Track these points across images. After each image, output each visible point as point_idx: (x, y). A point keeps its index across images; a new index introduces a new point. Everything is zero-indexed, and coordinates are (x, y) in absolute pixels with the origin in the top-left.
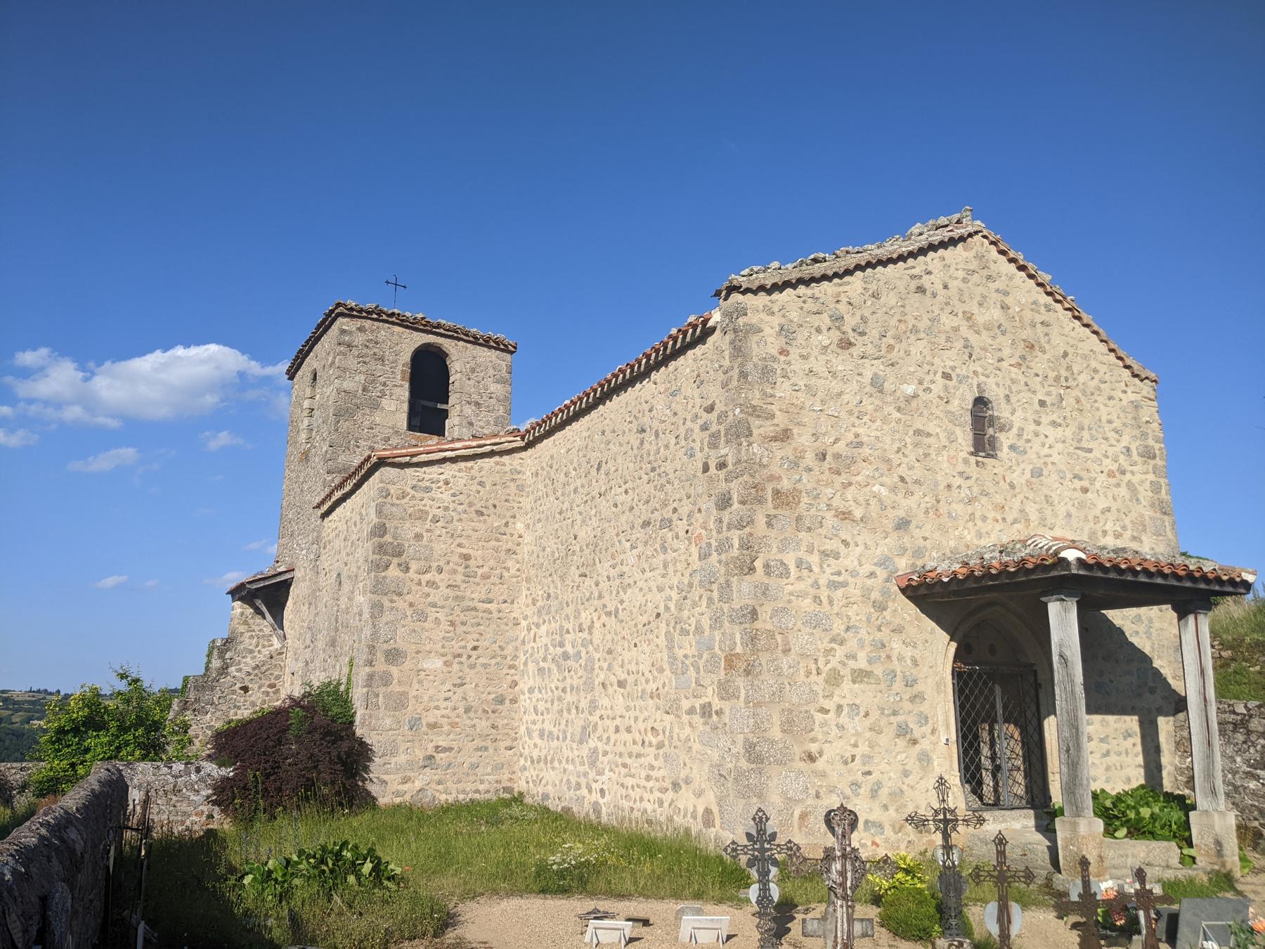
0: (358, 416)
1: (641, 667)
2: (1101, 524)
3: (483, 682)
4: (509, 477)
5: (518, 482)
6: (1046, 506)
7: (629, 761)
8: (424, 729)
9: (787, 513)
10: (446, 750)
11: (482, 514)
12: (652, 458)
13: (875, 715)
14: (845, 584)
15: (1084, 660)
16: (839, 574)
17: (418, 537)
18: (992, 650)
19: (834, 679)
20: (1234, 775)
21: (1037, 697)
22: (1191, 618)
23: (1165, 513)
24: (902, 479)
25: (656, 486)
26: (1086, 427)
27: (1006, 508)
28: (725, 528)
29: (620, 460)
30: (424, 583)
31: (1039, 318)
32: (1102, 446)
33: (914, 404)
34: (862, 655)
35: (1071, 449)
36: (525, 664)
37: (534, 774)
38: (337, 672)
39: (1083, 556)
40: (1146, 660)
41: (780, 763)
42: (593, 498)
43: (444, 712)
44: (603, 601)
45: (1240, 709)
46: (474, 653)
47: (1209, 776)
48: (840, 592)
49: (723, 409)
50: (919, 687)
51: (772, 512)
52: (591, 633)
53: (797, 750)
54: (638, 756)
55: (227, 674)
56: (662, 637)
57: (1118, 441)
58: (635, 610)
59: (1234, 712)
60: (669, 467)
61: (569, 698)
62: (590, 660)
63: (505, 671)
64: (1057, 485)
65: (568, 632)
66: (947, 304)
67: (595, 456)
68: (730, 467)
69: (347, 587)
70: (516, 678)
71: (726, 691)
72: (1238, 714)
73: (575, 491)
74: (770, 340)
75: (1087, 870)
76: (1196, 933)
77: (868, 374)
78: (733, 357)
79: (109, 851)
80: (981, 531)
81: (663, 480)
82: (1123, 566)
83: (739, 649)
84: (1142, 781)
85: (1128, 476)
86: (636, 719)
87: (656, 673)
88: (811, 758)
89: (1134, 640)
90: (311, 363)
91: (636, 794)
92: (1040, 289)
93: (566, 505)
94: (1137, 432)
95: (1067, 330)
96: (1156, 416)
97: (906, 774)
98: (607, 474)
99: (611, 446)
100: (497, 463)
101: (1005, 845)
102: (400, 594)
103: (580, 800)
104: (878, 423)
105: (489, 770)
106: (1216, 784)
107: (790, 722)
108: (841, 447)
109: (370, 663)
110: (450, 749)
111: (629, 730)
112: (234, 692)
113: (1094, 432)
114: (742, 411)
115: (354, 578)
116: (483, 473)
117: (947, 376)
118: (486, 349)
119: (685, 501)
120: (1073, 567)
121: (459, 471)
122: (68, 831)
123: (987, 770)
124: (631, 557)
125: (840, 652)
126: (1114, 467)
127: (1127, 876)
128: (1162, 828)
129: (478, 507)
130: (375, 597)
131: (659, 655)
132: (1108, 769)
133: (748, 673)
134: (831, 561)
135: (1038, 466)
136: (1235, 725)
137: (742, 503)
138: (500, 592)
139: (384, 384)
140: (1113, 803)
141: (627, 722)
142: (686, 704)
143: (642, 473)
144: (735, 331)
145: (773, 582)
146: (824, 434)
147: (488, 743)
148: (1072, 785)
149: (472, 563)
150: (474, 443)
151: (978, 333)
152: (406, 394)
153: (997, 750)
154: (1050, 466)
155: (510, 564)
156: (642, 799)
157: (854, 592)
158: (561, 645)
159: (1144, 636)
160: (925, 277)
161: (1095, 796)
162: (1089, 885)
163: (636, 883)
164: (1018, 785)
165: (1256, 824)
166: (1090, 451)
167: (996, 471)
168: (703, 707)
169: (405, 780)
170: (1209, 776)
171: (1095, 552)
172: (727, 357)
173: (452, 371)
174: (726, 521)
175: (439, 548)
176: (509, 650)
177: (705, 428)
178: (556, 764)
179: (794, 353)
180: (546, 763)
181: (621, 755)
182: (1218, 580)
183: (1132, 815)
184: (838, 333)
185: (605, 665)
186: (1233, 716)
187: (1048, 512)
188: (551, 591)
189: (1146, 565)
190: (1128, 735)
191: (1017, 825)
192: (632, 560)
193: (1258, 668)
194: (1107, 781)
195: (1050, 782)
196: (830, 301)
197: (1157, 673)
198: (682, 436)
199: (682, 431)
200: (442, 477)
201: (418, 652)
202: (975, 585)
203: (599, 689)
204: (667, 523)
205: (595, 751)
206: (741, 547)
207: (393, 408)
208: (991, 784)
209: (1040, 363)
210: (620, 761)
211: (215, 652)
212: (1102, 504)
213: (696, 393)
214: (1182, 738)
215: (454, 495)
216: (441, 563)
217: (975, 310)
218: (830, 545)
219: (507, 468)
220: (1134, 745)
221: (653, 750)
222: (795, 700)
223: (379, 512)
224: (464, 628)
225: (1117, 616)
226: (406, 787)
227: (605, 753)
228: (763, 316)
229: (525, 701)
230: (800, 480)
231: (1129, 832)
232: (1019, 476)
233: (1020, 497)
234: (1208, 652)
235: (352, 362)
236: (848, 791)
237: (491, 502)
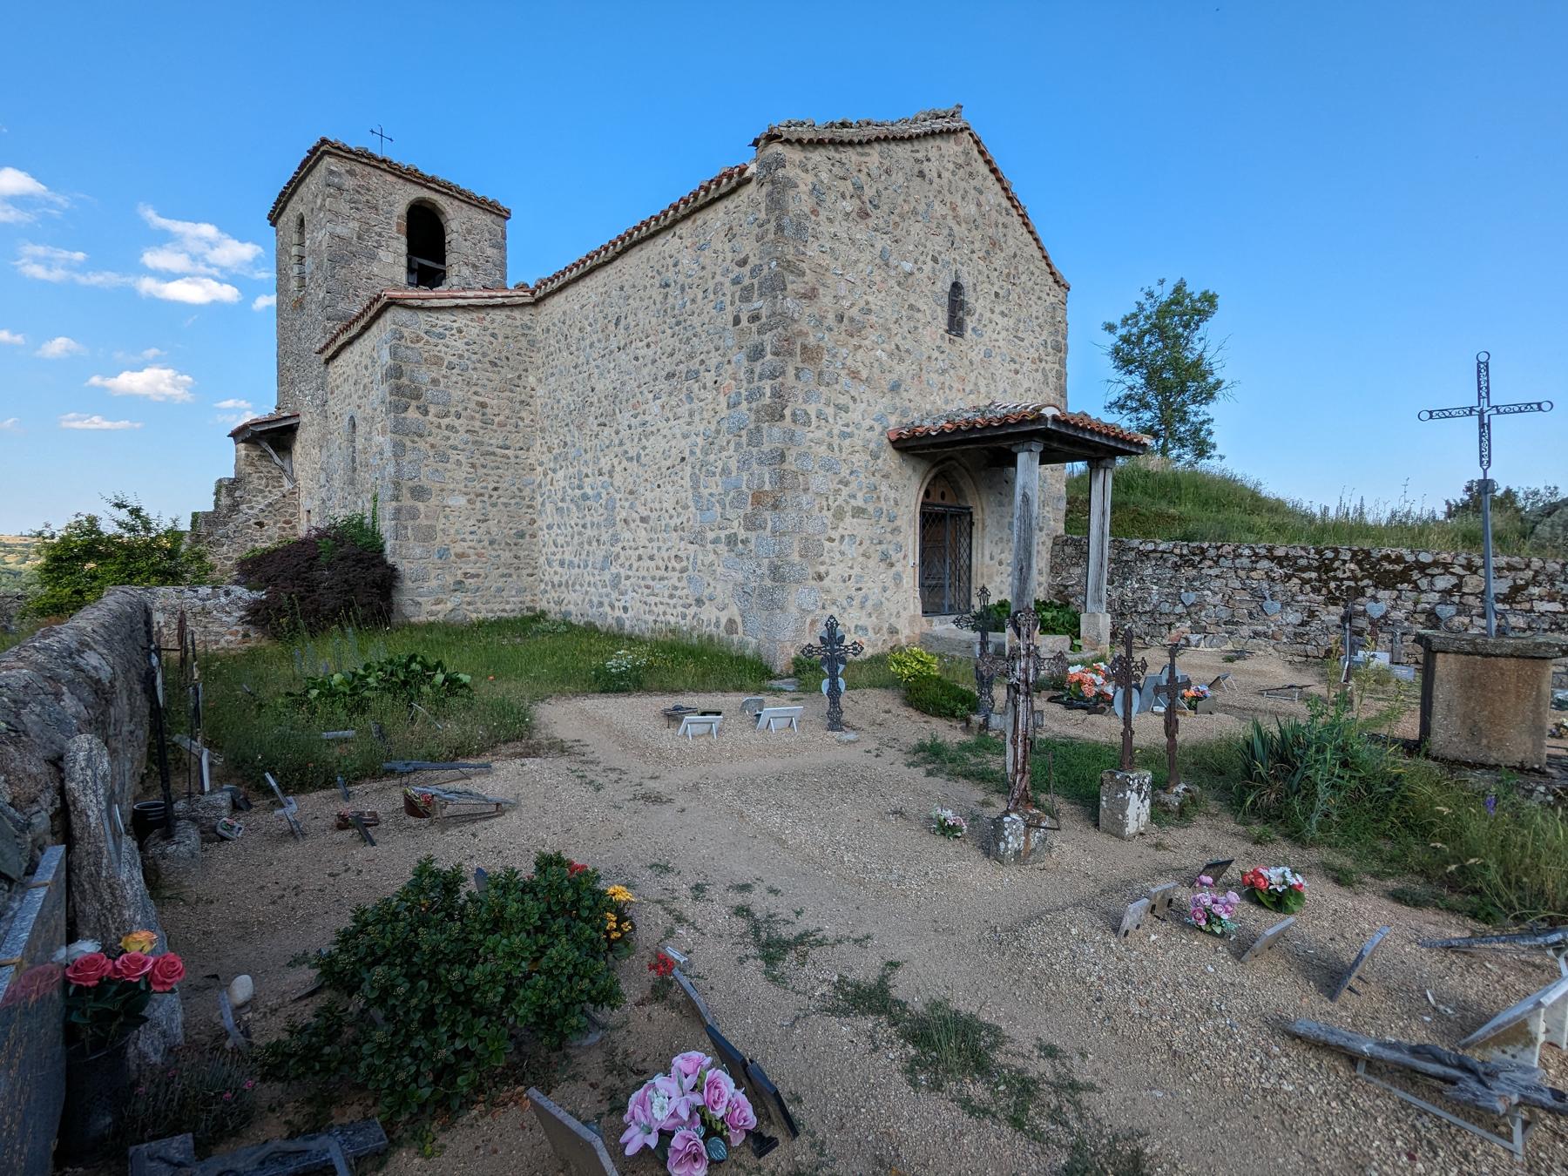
0: (355, 264)
1: (665, 505)
3: (505, 519)
4: (519, 331)
5: (529, 338)
7: (651, 583)
8: (453, 558)
9: (812, 368)
10: (473, 576)
11: (496, 365)
12: (676, 312)
13: (867, 543)
14: (850, 435)
16: (847, 425)
17: (435, 382)
19: (839, 514)
24: (897, 347)
25: (681, 340)
28: (756, 378)
29: (641, 315)
30: (443, 427)
31: (1001, 220)
33: (910, 281)
34: (860, 495)
36: (543, 504)
37: (556, 596)
38: (363, 506)
39: (1058, 413)
41: (798, 582)
42: (612, 352)
43: (471, 544)
44: (624, 447)
46: (495, 494)
48: (848, 441)
49: (758, 262)
50: (897, 523)
51: (800, 365)
52: (611, 477)
53: (810, 571)
54: (661, 579)
55: (239, 511)
56: (688, 478)
58: (658, 456)
60: (695, 320)
61: (589, 532)
62: (611, 499)
63: (524, 510)
65: (587, 476)
66: (940, 192)
67: (612, 312)
68: (764, 320)
69: (362, 428)
70: (534, 516)
71: (752, 523)
73: (592, 345)
74: (804, 197)
77: (879, 246)
78: (769, 210)
79: (154, 679)
81: (689, 333)
83: (767, 487)
86: (659, 548)
87: (680, 510)
88: (820, 578)
90: (295, 207)
91: (661, 609)
92: (1002, 192)
93: (582, 359)
94: (1052, 329)
95: (1019, 233)
97: (885, 589)
98: (626, 329)
99: (631, 301)
100: (508, 317)
102: (421, 436)
103: (604, 616)
104: (883, 294)
105: (514, 593)
107: (806, 548)
108: (854, 312)
109: (396, 498)
110: (478, 576)
111: (651, 558)
112: (249, 527)
114: (778, 265)
115: (370, 420)
116: (495, 325)
117: (935, 260)
118: (481, 211)
119: (713, 353)
121: (472, 320)
122: (85, 656)
124: (655, 407)
125: (845, 491)
129: (491, 357)
130: (398, 437)
131: (684, 494)
133: (775, 507)
134: (843, 414)
137: (776, 354)
138: (516, 440)
139: (380, 235)
141: (649, 552)
142: (710, 535)
143: (666, 326)
144: (773, 182)
145: (798, 429)
146: (843, 298)
147: (512, 571)
149: (488, 410)
150: (486, 294)
151: (959, 223)
152: (404, 249)
155: (524, 414)
156: (665, 613)
157: (859, 443)
158: (580, 487)
160: (925, 163)
163: (685, 681)
166: (1022, 340)
168: (728, 537)
169: (438, 602)
172: (763, 210)
173: (448, 231)
174: (758, 370)
175: (456, 394)
176: (527, 492)
177: (736, 281)
178: (578, 587)
179: (823, 214)
180: (567, 587)
181: (644, 578)
184: (858, 202)
185: (627, 504)
188: (568, 439)
192: (656, 410)
196: (853, 168)
198: (711, 290)
199: (711, 285)
200: (455, 325)
201: (442, 490)
203: (620, 525)
204: (694, 375)
205: (618, 576)
206: (773, 395)
207: (390, 260)
209: (999, 261)
210: (643, 583)
211: (224, 491)
213: (727, 246)
215: (467, 344)
216: (459, 409)
217: (959, 202)
218: (844, 400)
219: (518, 323)
221: (677, 574)
222: (811, 531)
223: (394, 354)
224: (485, 471)
226: (439, 607)
227: (628, 577)
228: (799, 171)
229: (544, 536)
232: (976, 356)
235: (344, 208)
236: (845, 603)
237: (504, 354)
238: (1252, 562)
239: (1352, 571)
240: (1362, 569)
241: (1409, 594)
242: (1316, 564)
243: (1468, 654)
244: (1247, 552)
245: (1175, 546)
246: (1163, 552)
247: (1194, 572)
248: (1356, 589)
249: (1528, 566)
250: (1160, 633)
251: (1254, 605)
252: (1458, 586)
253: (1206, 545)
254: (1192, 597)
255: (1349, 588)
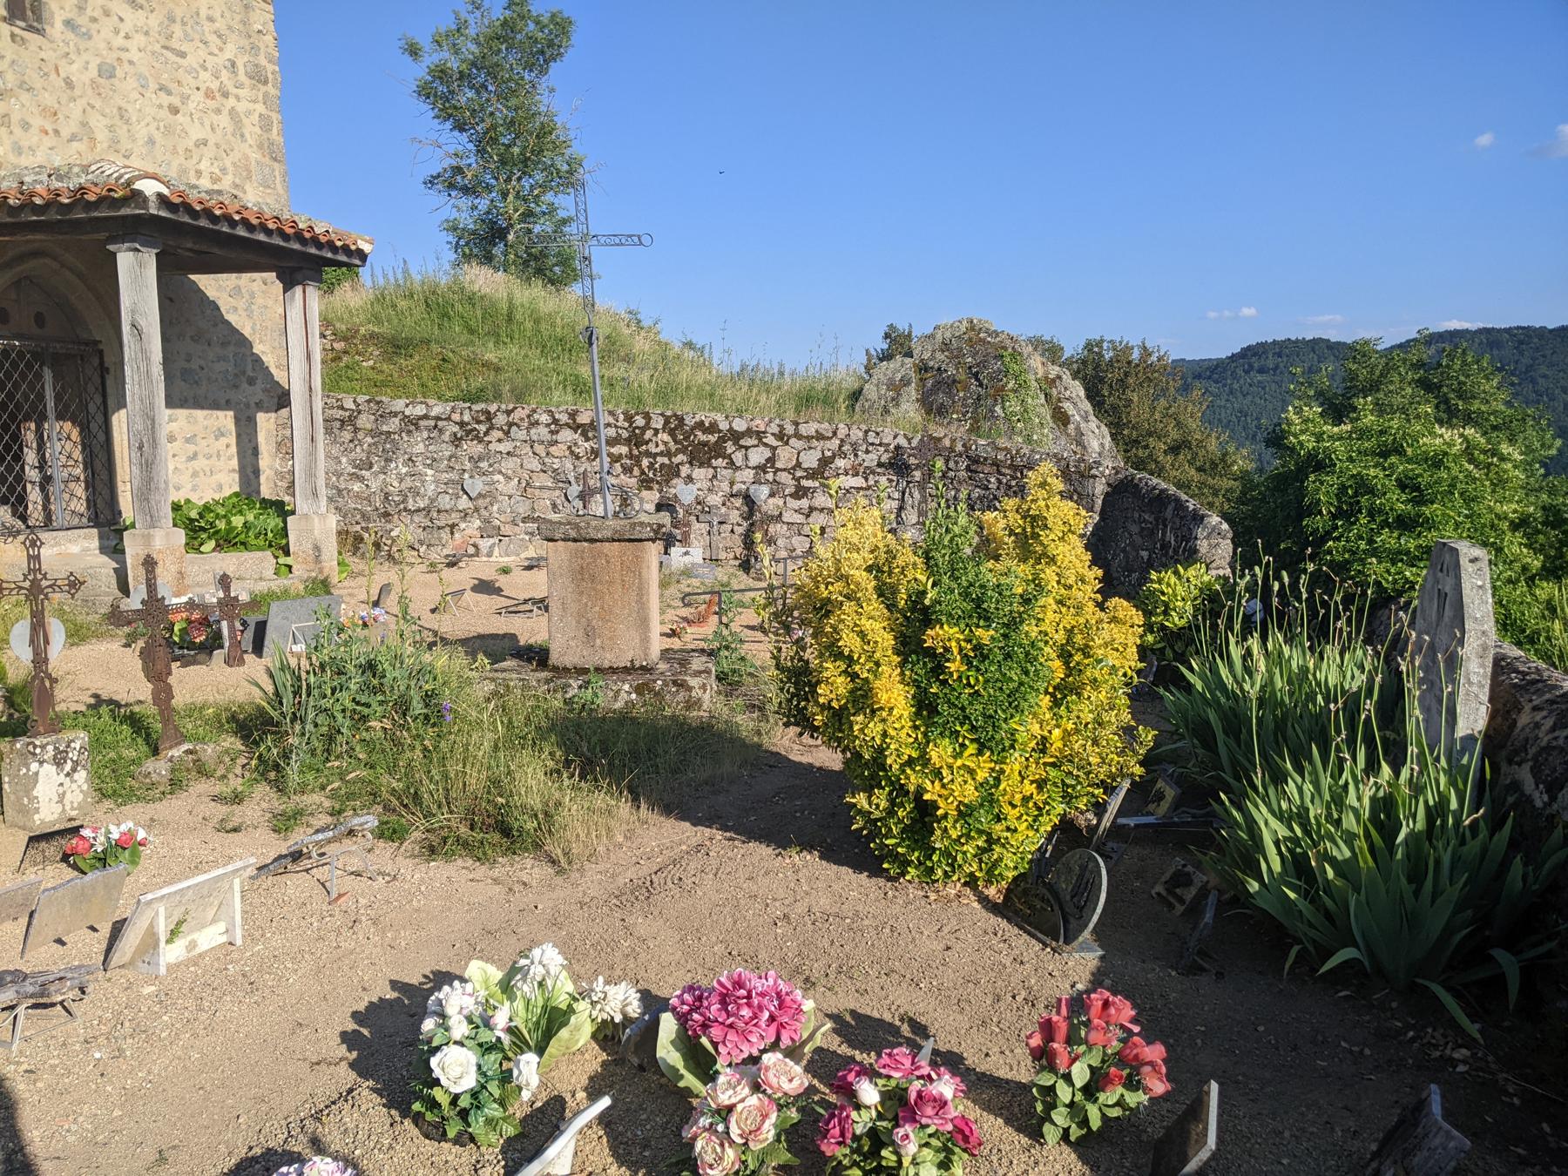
2: (194, 161)
6: (119, 123)
15: (165, 339)
18: (40, 320)
20: (338, 479)
21: (103, 384)
22: (298, 290)
23: (275, 160)
26: (178, 20)
27: (60, 115)
32: (201, 53)
35: (157, 47)
39: (166, 191)
40: (244, 343)
45: (349, 404)
47: (311, 474)
57: (221, 50)
59: (342, 408)
64: (134, 95)
72: (346, 410)
75: (153, 571)
76: (285, 637)
80: (21, 143)
82: (218, 212)
84: (237, 489)
85: (232, 102)
89: (230, 317)
94: (245, 42)
96: (271, 27)
101: (39, 548)
106: (318, 485)
113: (188, 28)
120: (151, 204)
123: (33, 483)
126: (215, 85)
127: (208, 584)
128: (257, 537)
132: (195, 474)
135: (108, 61)
136: (342, 421)
140: (200, 514)
148: (145, 494)
153: (47, 455)
154: (126, 66)
159: (244, 314)
161: (176, 507)
162: (155, 589)
164: (76, 499)
165: (358, 528)
166: (183, 55)
167: (43, 55)
170: (311, 474)
171: (181, 189)
182: (331, 245)
183: (221, 525)
186: (341, 412)
187: (122, 131)
189: (246, 214)
190: (220, 434)
191: (75, 549)
193: (371, 363)
194: (194, 489)
195: (120, 493)
197: (258, 360)
202: (9, 220)
208: (39, 500)
212: (196, 133)
214: (285, 437)
220: (227, 446)
225: (213, 285)
231: (218, 545)
232: (81, 70)
233: (81, 103)
234: (317, 346)
238: (552, 432)
239: (666, 443)
240: (676, 442)
241: (725, 472)
242: (625, 434)
243: (575, 540)
244: (545, 418)
245: (453, 410)
246: (438, 418)
247: (480, 448)
248: (670, 466)
249: (835, 433)
250: (440, 539)
251: (557, 493)
252: (771, 460)
253: (493, 408)
254: (476, 485)
255: (662, 465)
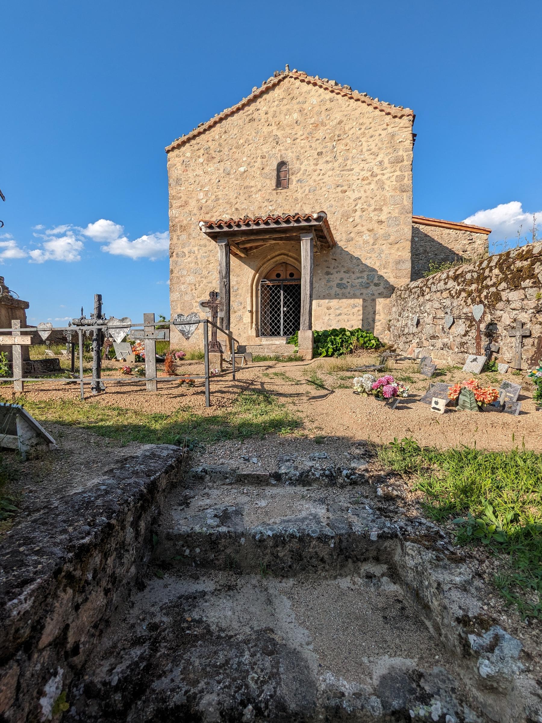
51: (179, 234)
74: (179, 168)
145: (179, 259)
230: (191, 219)
